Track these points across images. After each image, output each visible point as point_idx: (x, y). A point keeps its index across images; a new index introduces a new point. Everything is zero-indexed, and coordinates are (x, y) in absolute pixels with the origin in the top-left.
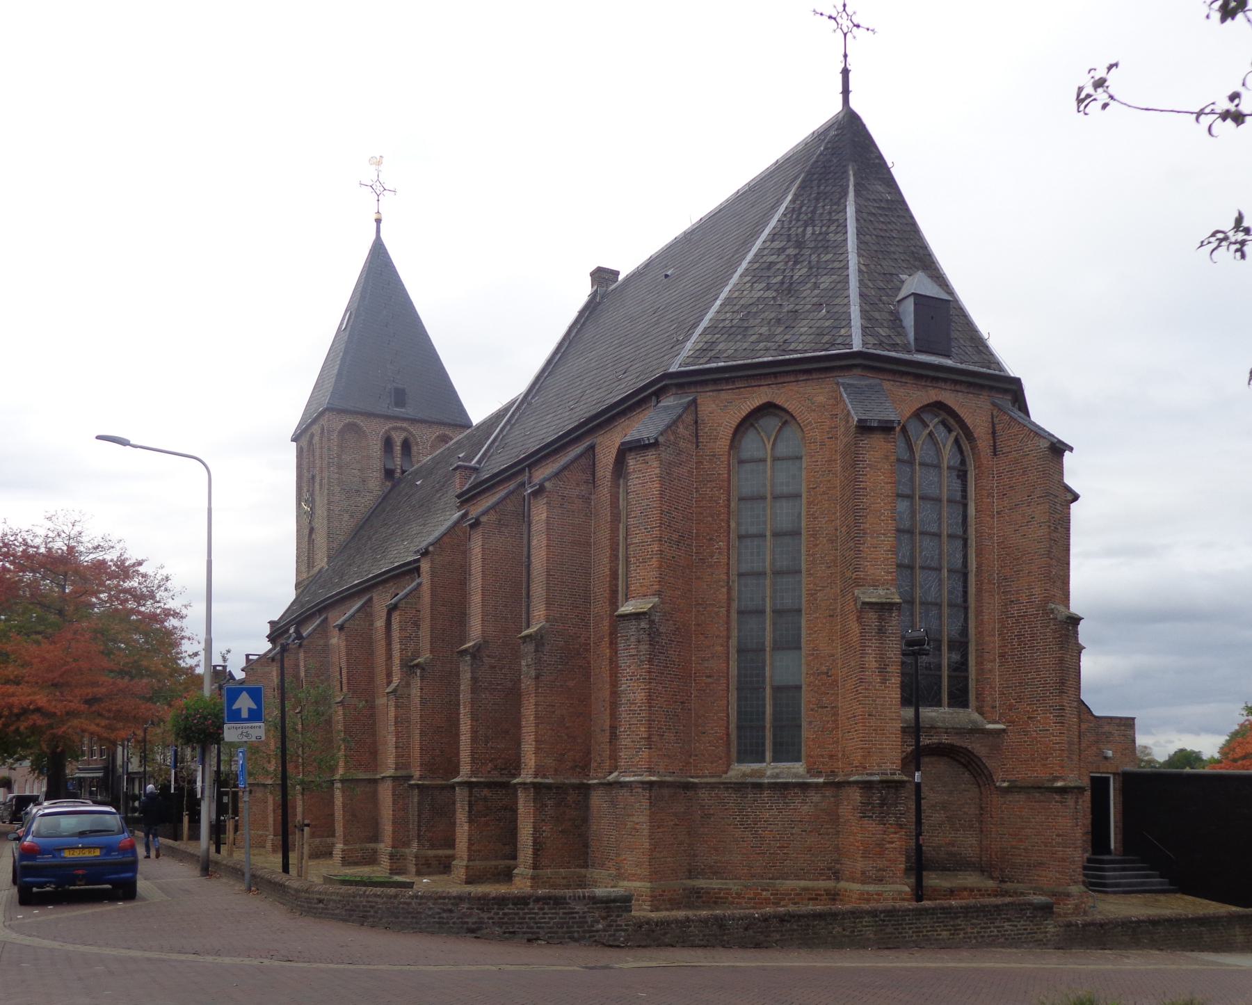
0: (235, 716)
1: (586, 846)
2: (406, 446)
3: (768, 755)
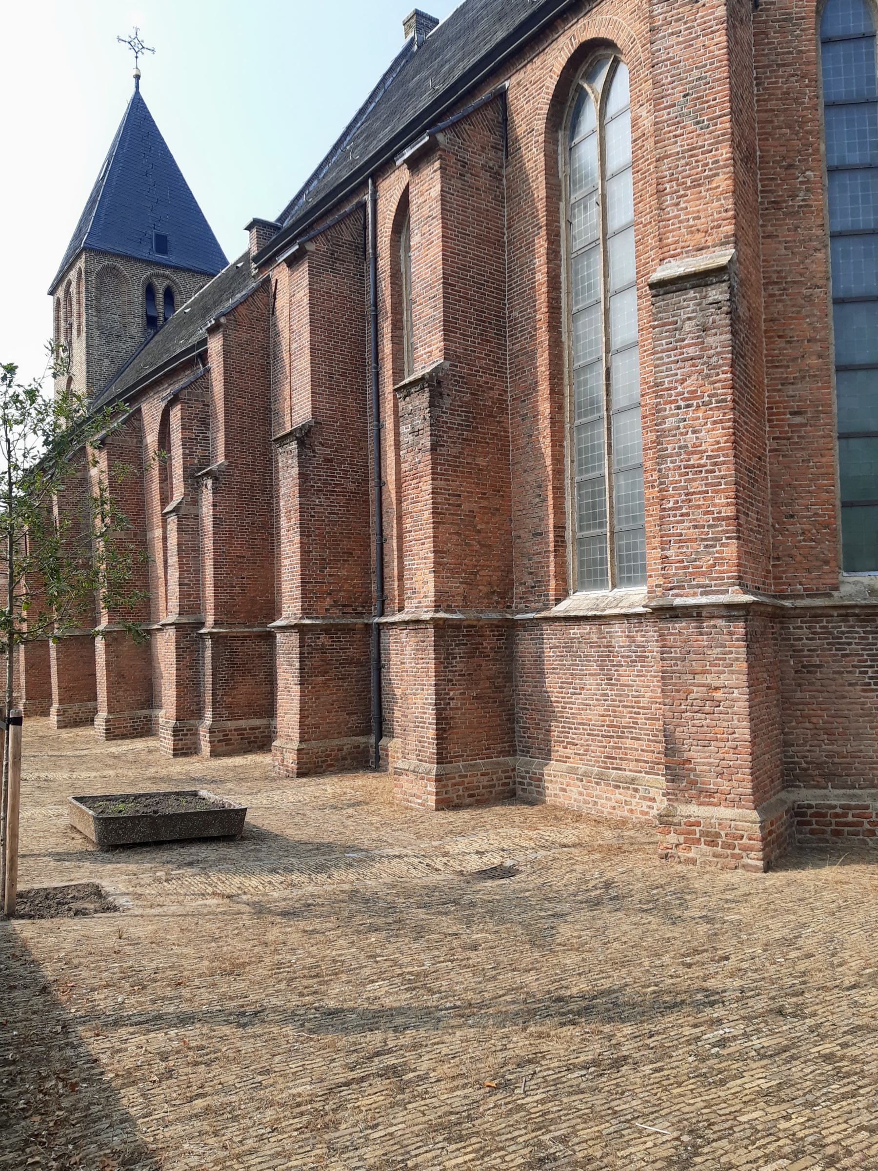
1: (512, 719)
2: (169, 295)
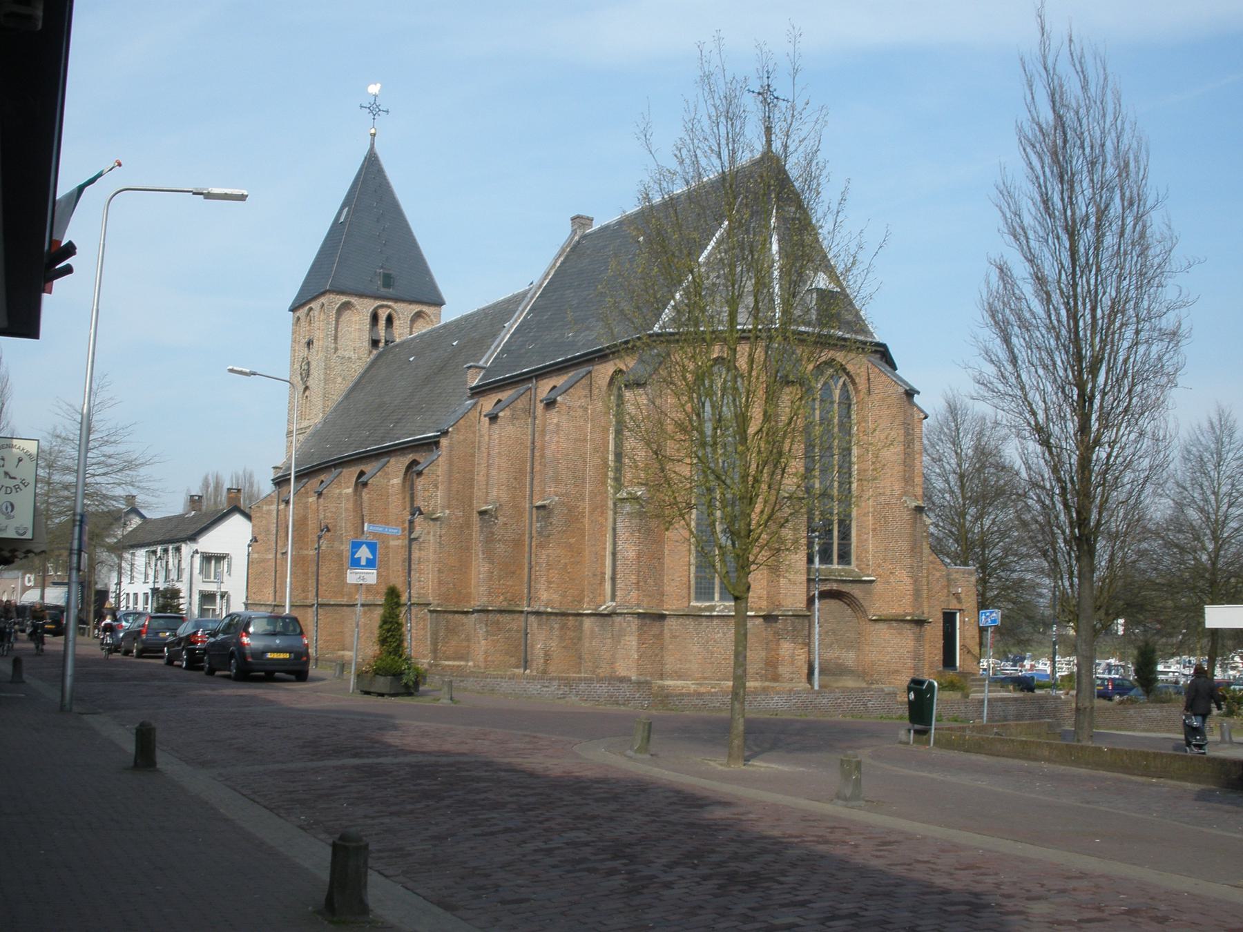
0: (356, 563)
2: (390, 320)
3: (717, 596)
